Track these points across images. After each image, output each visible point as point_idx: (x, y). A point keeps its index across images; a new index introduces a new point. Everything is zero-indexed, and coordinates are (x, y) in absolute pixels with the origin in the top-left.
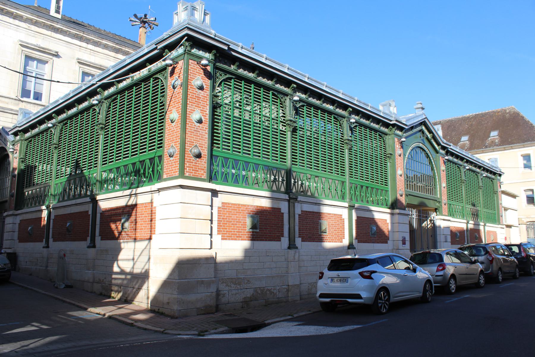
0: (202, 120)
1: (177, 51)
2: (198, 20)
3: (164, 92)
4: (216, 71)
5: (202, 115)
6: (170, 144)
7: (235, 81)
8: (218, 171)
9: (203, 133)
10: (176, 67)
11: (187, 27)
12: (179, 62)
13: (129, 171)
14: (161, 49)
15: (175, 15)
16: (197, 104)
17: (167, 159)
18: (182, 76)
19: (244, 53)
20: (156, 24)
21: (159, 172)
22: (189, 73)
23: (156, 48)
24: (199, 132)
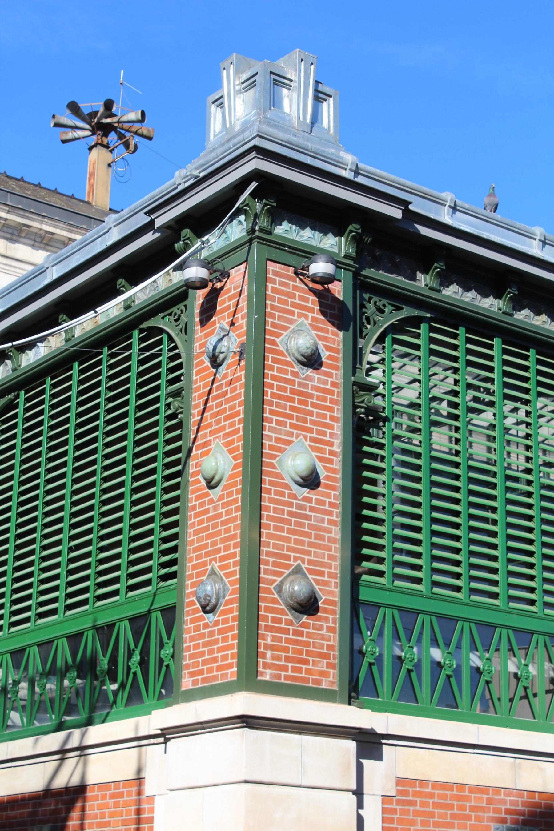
0: (317, 476)
1: (224, 232)
2: (295, 120)
3: (177, 379)
4: (362, 299)
5: (318, 457)
6: (205, 564)
7: (432, 329)
8: (379, 659)
9: (322, 521)
10: (222, 288)
11: (255, 148)
12: (232, 272)
13: (59, 662)
14: (167, 226)
15: (213, 107)
16: (298, 419)
17: (193, 621)
18: (245, 321)
19: (463, 227)
20: (145, 132)
21: (164, 668)
22: (268, 310)
23: (148, 227)
24: (308, 517)
